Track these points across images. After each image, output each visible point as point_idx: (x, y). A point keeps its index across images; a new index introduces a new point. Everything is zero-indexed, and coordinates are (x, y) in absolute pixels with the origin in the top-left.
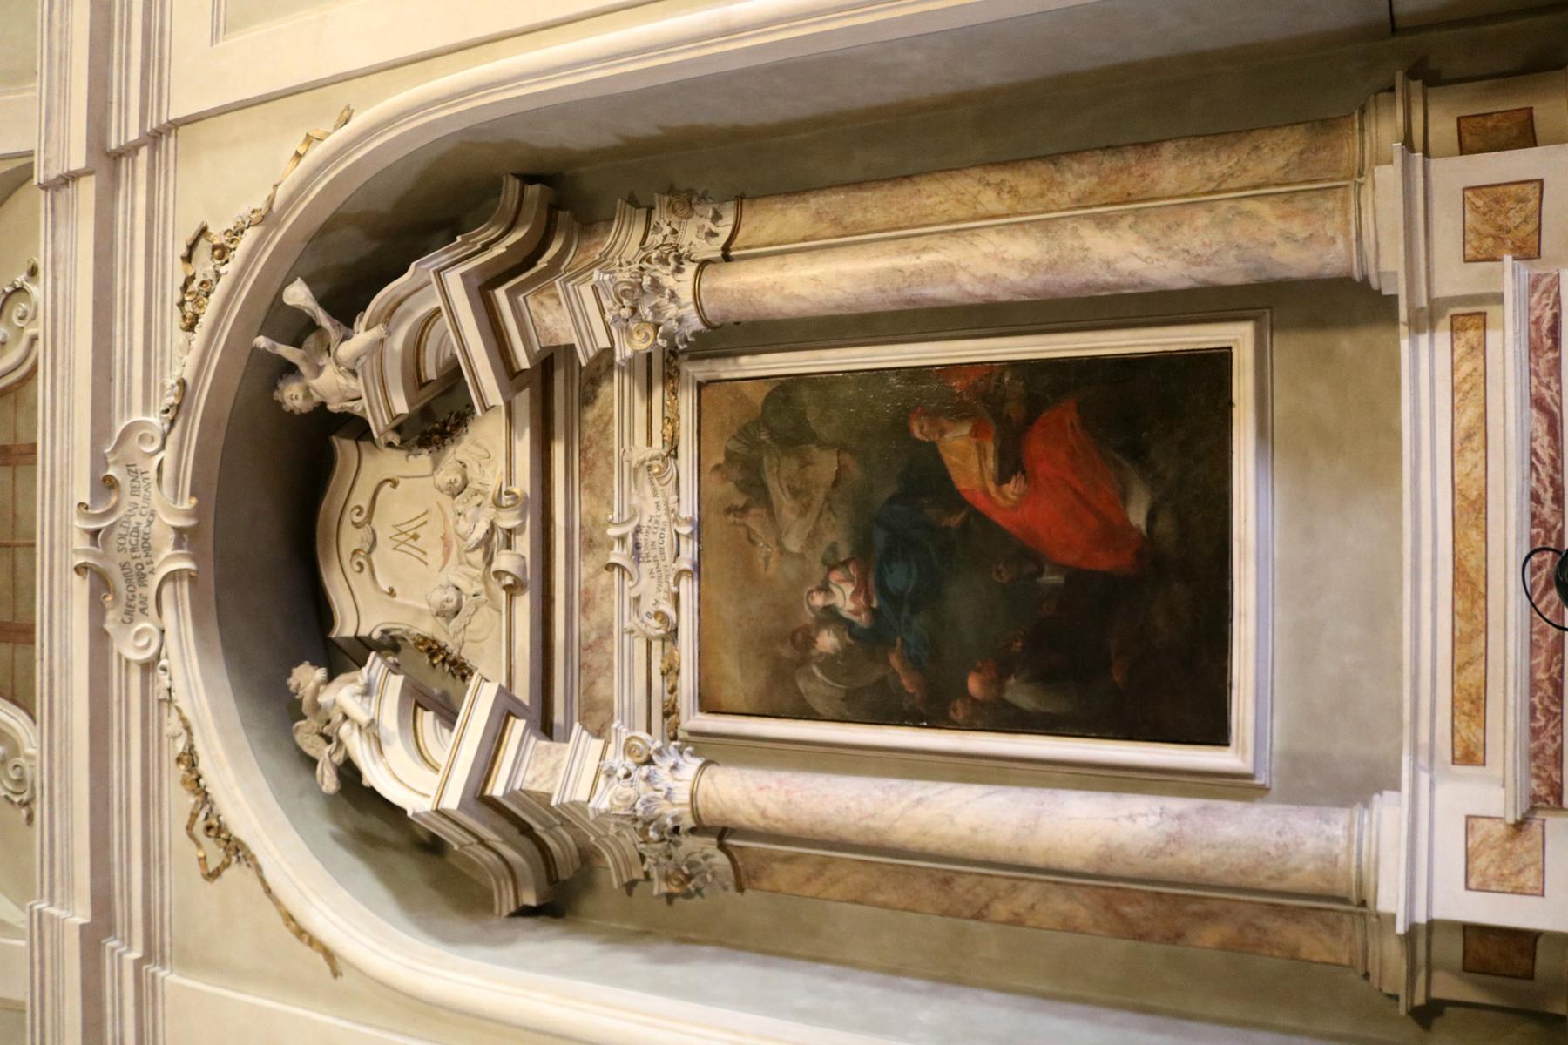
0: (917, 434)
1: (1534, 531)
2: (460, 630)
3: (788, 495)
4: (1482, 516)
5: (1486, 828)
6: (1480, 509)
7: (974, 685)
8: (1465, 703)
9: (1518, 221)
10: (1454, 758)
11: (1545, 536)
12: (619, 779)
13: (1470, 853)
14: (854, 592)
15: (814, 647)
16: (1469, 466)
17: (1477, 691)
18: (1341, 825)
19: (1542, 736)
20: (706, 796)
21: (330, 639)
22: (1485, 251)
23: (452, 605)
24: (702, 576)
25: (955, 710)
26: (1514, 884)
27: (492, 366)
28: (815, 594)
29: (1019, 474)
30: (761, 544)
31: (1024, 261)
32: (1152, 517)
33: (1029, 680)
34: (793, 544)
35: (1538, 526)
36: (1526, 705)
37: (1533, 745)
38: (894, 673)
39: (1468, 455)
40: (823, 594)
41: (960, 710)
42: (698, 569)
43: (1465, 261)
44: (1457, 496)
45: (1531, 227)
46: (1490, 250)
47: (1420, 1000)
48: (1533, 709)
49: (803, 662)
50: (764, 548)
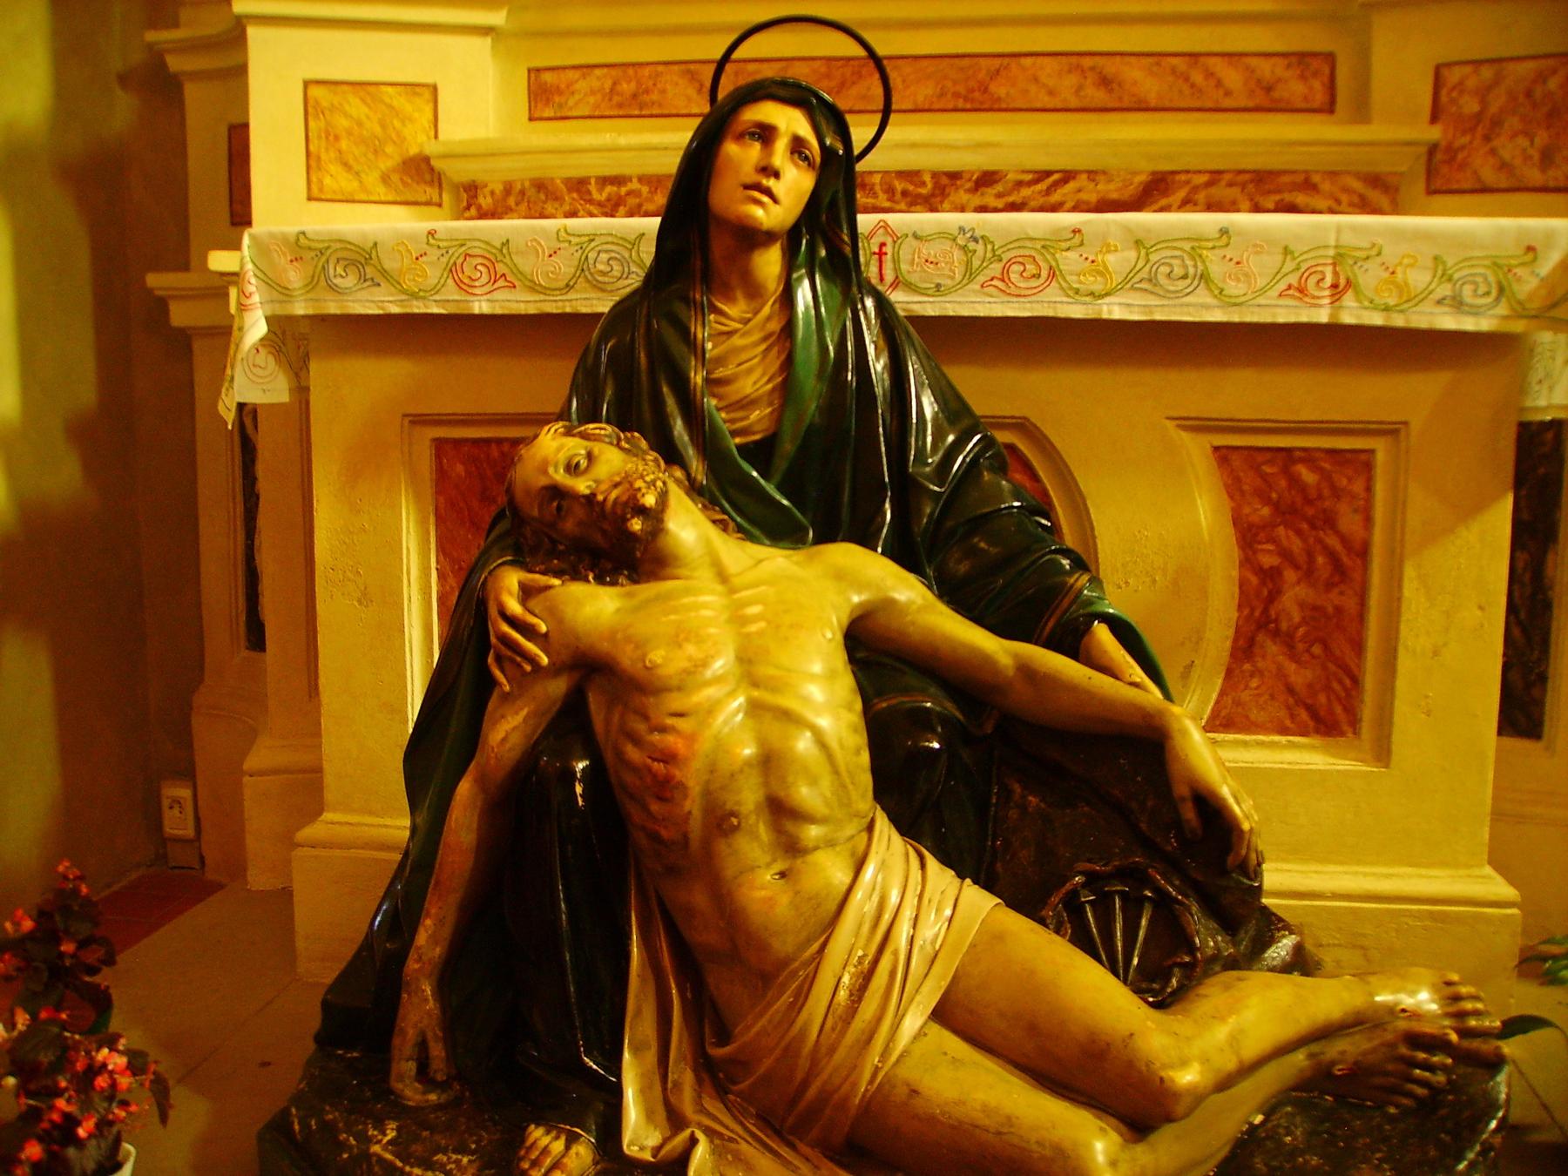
1: (927, 178)
4: (960, 104)
5: (416, 115)
6: (973, 101)
8: (633, 85)
9: (1506, 154)
10: (538, 70)
11: (919, 196)
13: (371, 89)
16: (1051, 82)
19: (575, 195)
22: (1453, 101)
26: (324, 156)
35: (936, 185)
36: (626, 171)
37: (558, 181)
39: (1071, 81)
44: (997, 62)
45: (1489, 175)
46: (1454, 109)
47: (175, 63)
48: (618, 180)
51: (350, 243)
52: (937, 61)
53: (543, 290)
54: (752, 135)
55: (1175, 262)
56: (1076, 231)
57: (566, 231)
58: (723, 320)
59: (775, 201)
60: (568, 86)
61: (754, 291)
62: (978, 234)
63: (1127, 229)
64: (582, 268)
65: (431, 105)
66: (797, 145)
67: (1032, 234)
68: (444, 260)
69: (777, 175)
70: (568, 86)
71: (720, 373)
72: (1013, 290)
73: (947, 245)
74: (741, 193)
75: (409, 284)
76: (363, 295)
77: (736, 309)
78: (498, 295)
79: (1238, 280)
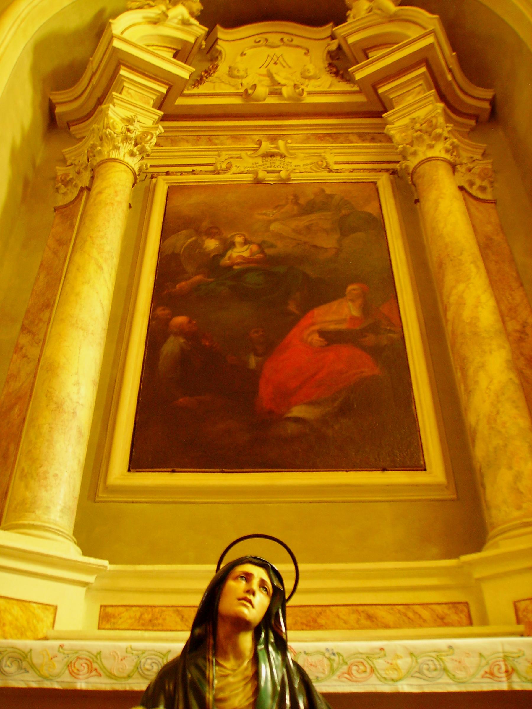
0: (350, 287)
2: (221, 80)
3: (306, 224)
7: (180, 320)
8: (150, 616)
10: (105, 606)
12: (127, 126)
13: (26, 604)
14: (243, 256)
15: (208, 238)
16: (345, 618)
17: (159, 624)
18: (58, 519)
20: (114, 166)
21: (216, 25)
23: (235, 73)
24: (256, 185)
25: (164, 310)
27: (379, 70)
28: (242, 238)
29: (326, 342)
30: (274, 212)
31: (477, 318)
32: (297, 420)
33: (182, 349)
34: (274, 227)
38: (190, 278)
39: (354, 617)
40: (243, 241)
41: (163, 312)
42: (258, 182)
43: (515, 604)
44: (320, 609)
46: (526, 620)
49: (198, 232)
50: (272, 214)
51: (17, 649)
52: (293, 608)
53: (116, 678)
54: (242, 577)
55: (430, 663)
56: (382, 649)
57: (131, 648)
58: (223, 669)
59: (253, 606)
60: (119, 615)
61: (239, 655)
62: (335, 651)
63: (406, 648)
64: (138, 667)
65: (53, 615)
66: (262, 584)
67: (361, 651)
68: (66, 660)
69: (254, 594)
70: (119, 615)
71: (221, 695)
72: (354, 679)
73: (320, 657)
74: (236, 602)
75: (45, 672)
76: (19, 677)
77: (229, 664)
78: (92, 680)
79: (461, 670)
